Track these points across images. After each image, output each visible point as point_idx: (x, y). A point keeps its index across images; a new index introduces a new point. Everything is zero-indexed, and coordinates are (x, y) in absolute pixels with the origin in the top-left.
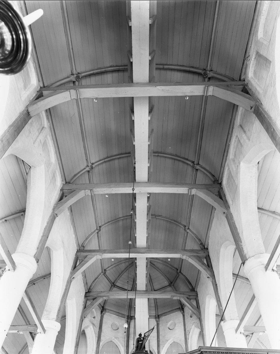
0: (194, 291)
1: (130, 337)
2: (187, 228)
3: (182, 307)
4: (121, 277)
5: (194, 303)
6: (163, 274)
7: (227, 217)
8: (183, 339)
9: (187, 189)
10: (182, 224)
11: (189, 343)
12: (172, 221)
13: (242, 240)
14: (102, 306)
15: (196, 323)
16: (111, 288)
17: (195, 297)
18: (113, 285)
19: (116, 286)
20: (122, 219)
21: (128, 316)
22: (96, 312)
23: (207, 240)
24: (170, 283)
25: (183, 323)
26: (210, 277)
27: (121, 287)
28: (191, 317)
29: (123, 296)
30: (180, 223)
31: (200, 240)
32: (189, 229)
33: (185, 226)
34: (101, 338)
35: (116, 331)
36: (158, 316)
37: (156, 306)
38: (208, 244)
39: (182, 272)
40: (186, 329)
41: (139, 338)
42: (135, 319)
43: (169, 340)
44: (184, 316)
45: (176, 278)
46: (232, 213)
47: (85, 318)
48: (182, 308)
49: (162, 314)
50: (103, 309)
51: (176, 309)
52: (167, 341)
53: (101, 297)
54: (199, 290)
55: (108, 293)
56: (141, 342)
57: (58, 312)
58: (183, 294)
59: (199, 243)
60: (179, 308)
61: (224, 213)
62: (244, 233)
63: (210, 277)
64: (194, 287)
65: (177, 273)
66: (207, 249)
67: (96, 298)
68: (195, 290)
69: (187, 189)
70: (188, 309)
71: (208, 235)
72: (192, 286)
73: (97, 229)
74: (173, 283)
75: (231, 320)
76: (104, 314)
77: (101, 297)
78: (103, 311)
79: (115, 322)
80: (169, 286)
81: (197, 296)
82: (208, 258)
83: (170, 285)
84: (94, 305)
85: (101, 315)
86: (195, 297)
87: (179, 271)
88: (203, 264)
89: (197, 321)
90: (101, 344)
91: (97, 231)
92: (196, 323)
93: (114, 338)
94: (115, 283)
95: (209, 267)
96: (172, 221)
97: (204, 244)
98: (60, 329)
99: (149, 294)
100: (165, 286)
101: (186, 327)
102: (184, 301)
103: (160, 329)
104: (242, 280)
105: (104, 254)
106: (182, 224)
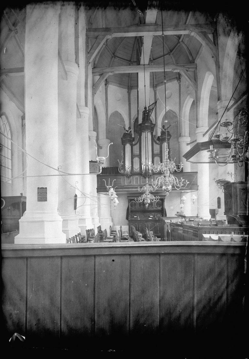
50: (107, 83)
60: (177, 78)
67: (102, 74)
70: (185, 78)
74: (173, 52)
95: (215, 45)
102: (182, 73)
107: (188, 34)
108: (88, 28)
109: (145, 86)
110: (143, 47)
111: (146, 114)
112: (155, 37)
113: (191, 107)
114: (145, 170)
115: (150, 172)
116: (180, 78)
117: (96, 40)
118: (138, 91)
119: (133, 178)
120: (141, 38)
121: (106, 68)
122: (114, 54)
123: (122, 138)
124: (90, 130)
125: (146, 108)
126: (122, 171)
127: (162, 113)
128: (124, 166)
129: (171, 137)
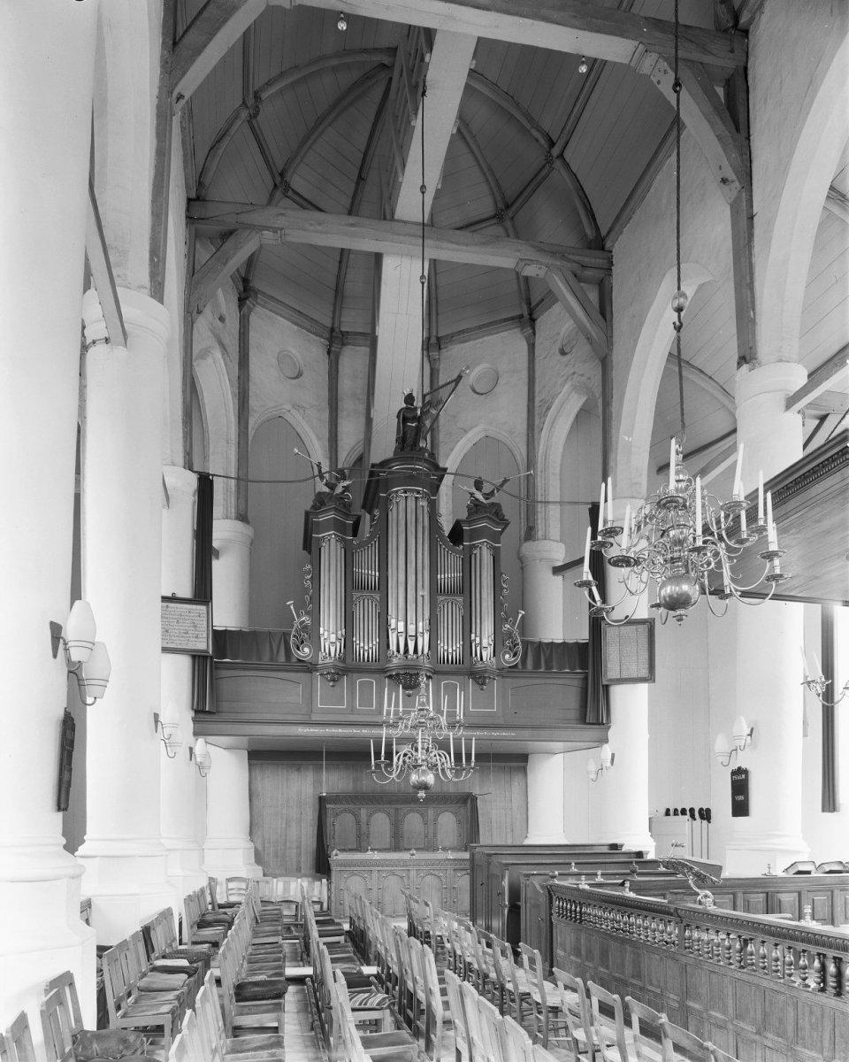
0: (603, 248)
3: (530, 314)
4: (310, 147)
5: (593, 296)
8: (522, 427)
11: (542, 442)
14: (503, 198)
15: (582, 375)
17: (598, 274)
18: (280, 185)
21: (332, 330)
22: (225, 299)
24: (501, 205)
25: (524, 375)
26: (734, 178)
28: (563, 353)
35: (294, 381)
36: (438, 339)
37: (434, 301)
39: (567, 155)
40: (534, 397)
41: (406, 408)
42: (372, 341)
45: (535, 182)
47: (199, 312)
49: (452, 335)
50: (246, 293)
51: (505, 320)
52: (466, 432)
54: (620, 247)
56: (414, 425)
58: (563, 257)
60: (521, 316)
64: (604, 233)
65: (549, 160)
66: (746, 33)
67: (231, 233)
68: (608, 245)
70: (560, 322)
72: (597, 229)
74: (514, 208)
75: (781, 361)
76: (250, 310)
78: (247, 298)
79: (289, 348)
80: (494, 221)
81: (609, 269)
83: (498, 217)
84: (228, 265)
85: (240, 312)
87: (556, 151)
90: (252, 422)
92: (582, 375)
93: (288, 407)
95: (738, 130)
99: (438, 239)
100: (477, 219)
101: (537, 389)
107: (626, 61)
110: (420, 116)
112: (485, 47)
116: (533, 321)
123: (307, 514)
124: (307, 860)
128: (311, 634)
129: (507, 525)
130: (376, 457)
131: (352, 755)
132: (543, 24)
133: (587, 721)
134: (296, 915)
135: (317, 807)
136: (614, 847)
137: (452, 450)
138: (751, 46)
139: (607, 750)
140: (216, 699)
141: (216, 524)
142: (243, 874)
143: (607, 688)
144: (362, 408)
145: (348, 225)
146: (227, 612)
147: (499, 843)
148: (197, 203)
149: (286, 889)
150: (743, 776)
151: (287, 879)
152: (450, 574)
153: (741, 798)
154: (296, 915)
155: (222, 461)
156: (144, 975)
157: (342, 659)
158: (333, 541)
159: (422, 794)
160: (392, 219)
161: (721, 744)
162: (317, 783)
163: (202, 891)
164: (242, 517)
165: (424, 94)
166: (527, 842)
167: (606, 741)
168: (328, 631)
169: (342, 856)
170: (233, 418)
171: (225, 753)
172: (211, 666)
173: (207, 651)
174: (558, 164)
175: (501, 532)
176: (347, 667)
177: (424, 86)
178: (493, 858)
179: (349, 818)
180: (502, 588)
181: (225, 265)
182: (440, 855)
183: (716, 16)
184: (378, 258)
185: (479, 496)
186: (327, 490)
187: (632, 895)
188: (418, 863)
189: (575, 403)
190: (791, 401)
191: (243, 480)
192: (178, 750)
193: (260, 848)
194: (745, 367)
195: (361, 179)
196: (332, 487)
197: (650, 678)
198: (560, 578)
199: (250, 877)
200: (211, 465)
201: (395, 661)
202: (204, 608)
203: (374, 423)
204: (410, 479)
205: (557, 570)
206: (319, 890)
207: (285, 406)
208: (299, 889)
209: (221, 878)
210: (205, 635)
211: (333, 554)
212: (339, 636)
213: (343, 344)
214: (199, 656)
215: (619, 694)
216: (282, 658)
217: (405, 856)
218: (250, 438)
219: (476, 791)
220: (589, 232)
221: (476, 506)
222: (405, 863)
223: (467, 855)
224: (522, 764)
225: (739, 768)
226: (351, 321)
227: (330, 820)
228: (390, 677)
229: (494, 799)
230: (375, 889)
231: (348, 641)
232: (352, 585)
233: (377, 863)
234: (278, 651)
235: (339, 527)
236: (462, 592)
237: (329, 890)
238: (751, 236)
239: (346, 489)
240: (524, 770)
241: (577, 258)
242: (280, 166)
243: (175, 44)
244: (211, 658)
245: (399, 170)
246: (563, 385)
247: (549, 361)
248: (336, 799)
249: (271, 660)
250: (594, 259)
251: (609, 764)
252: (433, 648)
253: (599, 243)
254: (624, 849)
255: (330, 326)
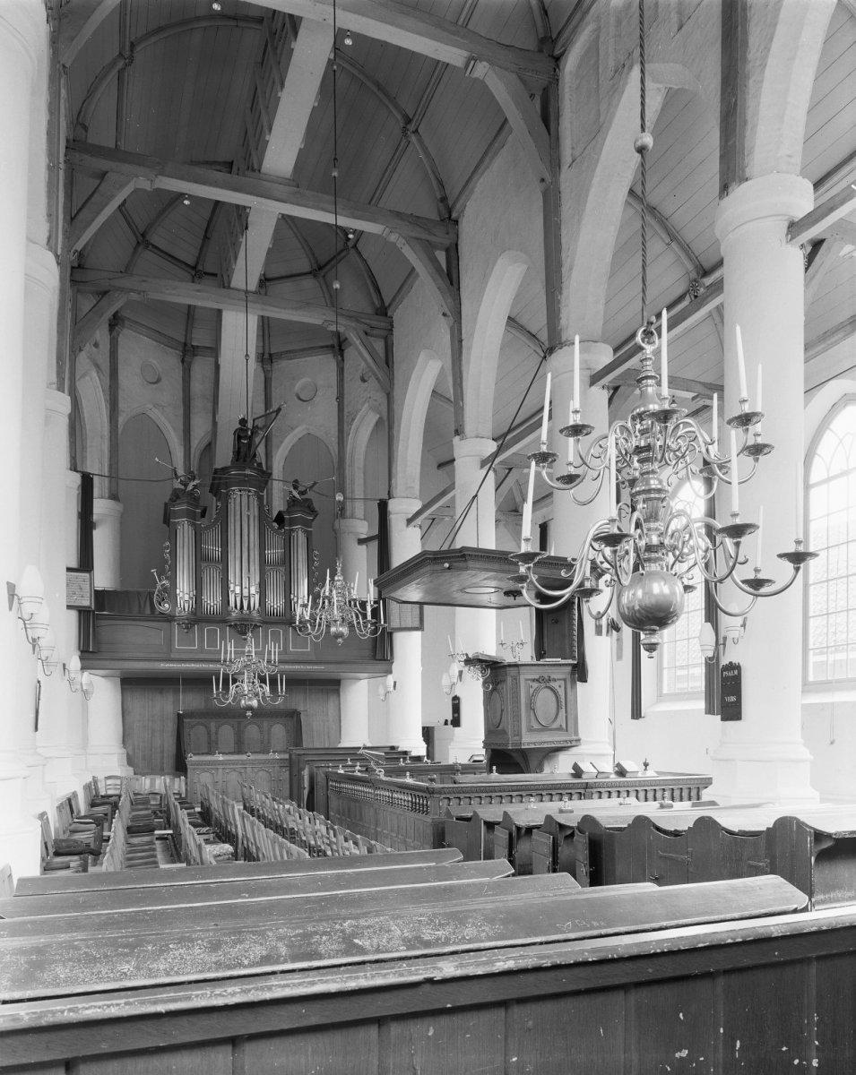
0: (386, 315)
1: (192, 405)
2: (412, 127)
3: (340, 346)
5: (379, 346)
6: (298, 234)
7: (545, 194)
8: (334, 431)
9: (466, 54)
10: (397, 106)
12: (369, 84)
13: (564, 286)
15: (376, 400)
16: (135, 249)
17: (384, 333)
19: (153, 245)
20: (205, 28)
21: (185, 344)
22: (101, 334)
23: (464, 197)
24: (315, 266)
27: (164, 249)
28: (363, 380)
29: (185, 294)
30: (393, 100)
31: (441, 183)
32: (416, 131)
33: (408, 121)
34: (120, 405)
35: (155, 386)
36: (270, 355)
37: (266, 326)
38: (463, 211)
39: (360, 246)
43: (297, 427)
44: (341, 371)
46: (561, 189)
47: (81, 350)
48: (338, 347)
49: (281, 353)
50: (115, 322)
51: (322, 347)
53: (122, 290)
54: (398, 315)
55: (144, 281)
57: (57, 362)
58: (358, 321)
59: (439, 197)
60: (333, 346)
61: (543, 180)
62: (574, 274)
63: (449, 313)
64: (387, 304)
66: (456, 222)
67: (105, 293)
69: (466, 54)
70: (359, 357)
71: (470, 186)
73: (121, 54)
74: (325, 270)
77: (122, 290)
82: (453, 252)
86: (384, 333)
88: (434, 261)
89: (380, 397)
90: (121, 420)
91: (120, 64)
92: (376, 400)
94: (148, 238)
95: (452, 284)
96: (369, 84)
97: (450, 203)
98: (70, 407)
102: (353, 338)
103: (273, 394)
104: (518, 334)
105: (160, 177)
106: (397, 106)
107: (380, 233)
108: (71, 137)
109: (247, 355)
111: (245, 438)
112: (285, 219)
113: (496, 528)
114: (238, 608)
115: (255, 614)
117: (98, 181)
118: (217, 367)
119: (201, 631)
120: (241, 212)
121: (120, 274)
122: (143, 235)
123: (166, 504)
124: (169, 762)
125: (246, 422)
126: (167, 605)
127: (289, 437)
128: (170, 593)
130: (219, 463)
131: (201, 682)
132: (322, 212)
133: (377, 658)
134: (160, 804)
135: (177, 721)
136: (393, 748)
137: (282, 442)
138: (460, 230)
139: (390, 679)
140: (97, 642)
141: (96, 502)
142: (118, 773)
143: (390, 635)
144: (210, 406)
145: (194, 290)
146: (103, 577)
147: (318, 747)
148: (79, 270)
149: (152, 784)
150: (736, 672)
151: (152, 777)
152: (273, 553)
153: (456, 715)
154: (160, 804)
155: (96, 463)
156: (70, 825)
157: (194, 613)
158: (186, 526)
159: (249, 713)
160: (229, 287)
161: (445, 681)
162: (176, 702)
163: (90, 783)
164: (114, 496)
165: (247, 228)
166: (339, 746)
167: (391, 672)
168: (183, 592)
169: (195, 758)
170: (106, 419)
171: (103, 679)
172: (93, 618)
173: (90, 607)
174: (352, 251)
175: (312, 520)
176: (198, 618)
177: (247, 224)
178: (302, 757)
179: (202, 729)
180: (314, 561)
181: (101, 317)
182: (271, 756)
183: (439, 211)
184: (220, 312)
185: (295, 493)
186: (183, 487)
187: (359, 774)
188: (253, 762)
189: (373, 418)
190: (409, 521)
191: (113, 476)
192: (52, 668)
193: (130, 753)
194: (457, 438)
195: (206, 238)
196: (186, 485)
197: (420, 628)
198: (364, 547)
199: (123, 775)
200: (88, 462)
201: (234, 614)
202: (87, 575)
203: (219, 426)
204: (243, 482)
205: (361, 542)
206: (179, 784)
207: (148, 406)
208: (160, 783)
209: (101, 776)
210: (88, 595)
211: (186, 535)
212: (191, 596)
213: (194, 355)
214: (84, 611)
215: (399, 638)
216: (148, 611)
217: (244, 757)
218: (120, 432)
219: (301, 708)
220: (377, 303)
221: (294, 501)
222: (243, 762)
223: (287, 756)
224: (337, 687)
225: (731, 663)
226: (200, 338)
227: (186, 731)
228: (230, 626)
229: (312, 710)
230: (221, 782)
231: (198, 598)
232: (201, 558)
233: (222, 763)
234: (145, 606)
235: (191, 516)
236: (284, 563)
237: (186, 784)
238: (461, 353)
239: (195, 487)
240: (337, 692)
241: (368, 321)
242: (142, 230)
243: (72, 219)
244: (94, 612)
245: (232, 261)
246: (363, 405)
247: (354, 388)
248: (190, 715)
249: (140, 612)
250: (380, 323)
251: (392, 689)
252: (263, 606)
253: (383, 311)
254: (400, 749)
255: (183, 341)
